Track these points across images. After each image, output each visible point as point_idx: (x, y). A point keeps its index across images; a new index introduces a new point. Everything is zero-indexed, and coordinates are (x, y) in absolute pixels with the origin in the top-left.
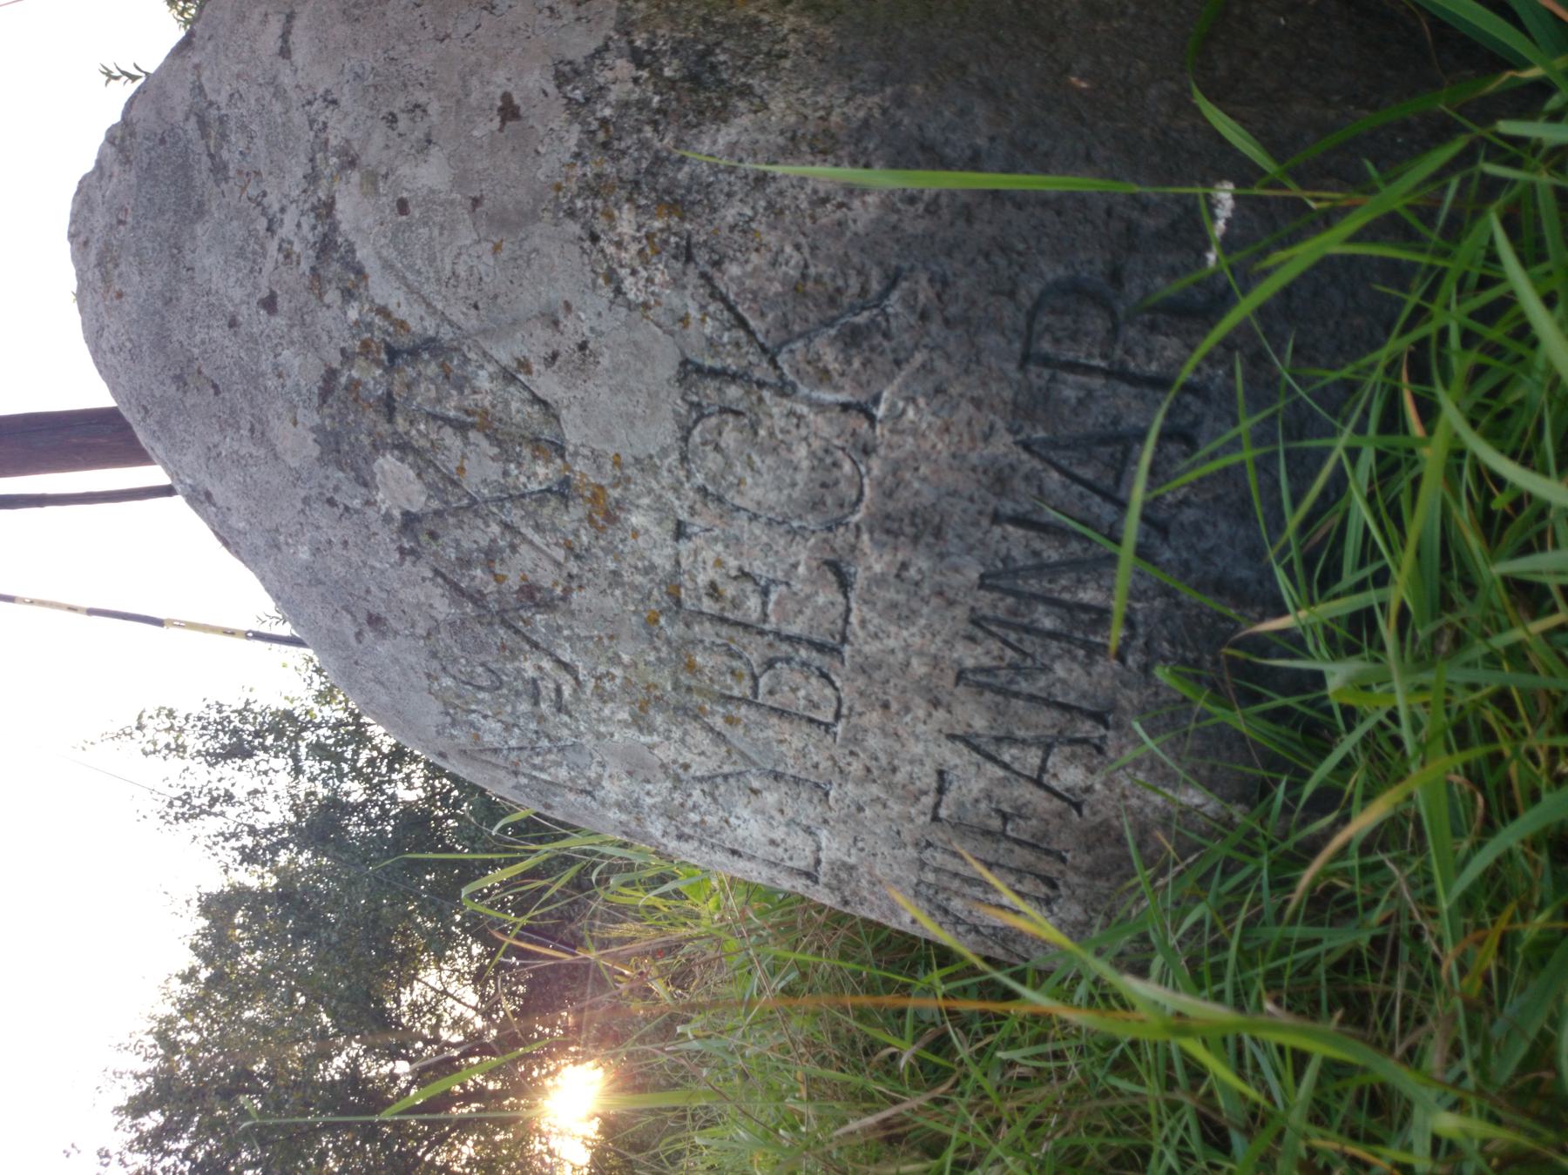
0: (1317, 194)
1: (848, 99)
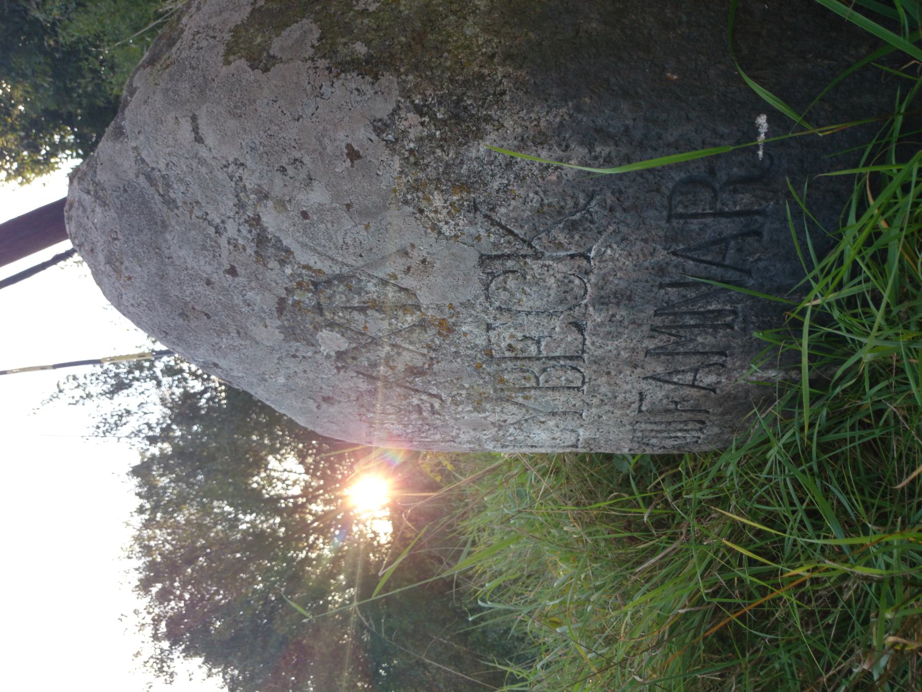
0: (822, 129)
1: (547, 113)
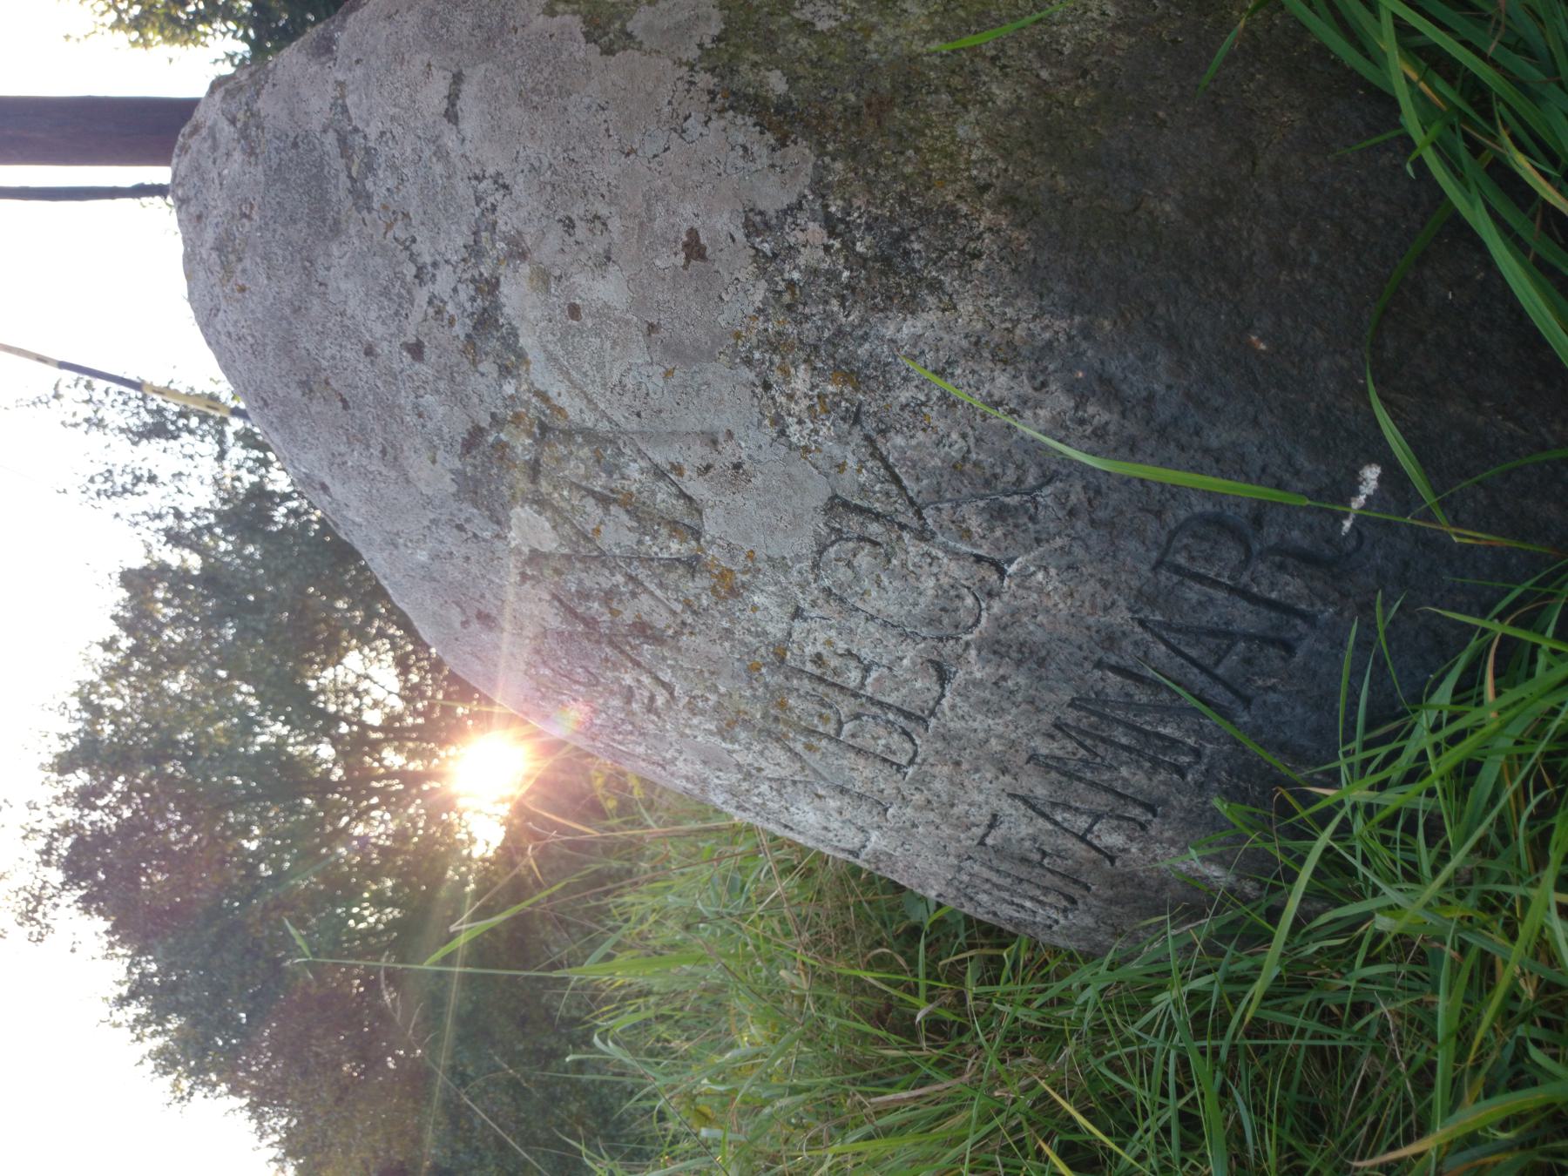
1: (1035, 317)
